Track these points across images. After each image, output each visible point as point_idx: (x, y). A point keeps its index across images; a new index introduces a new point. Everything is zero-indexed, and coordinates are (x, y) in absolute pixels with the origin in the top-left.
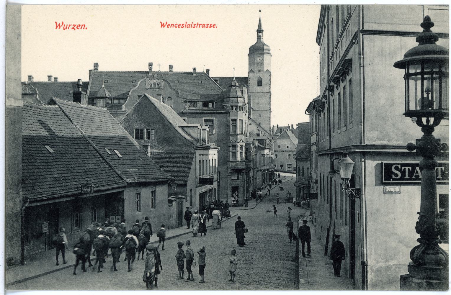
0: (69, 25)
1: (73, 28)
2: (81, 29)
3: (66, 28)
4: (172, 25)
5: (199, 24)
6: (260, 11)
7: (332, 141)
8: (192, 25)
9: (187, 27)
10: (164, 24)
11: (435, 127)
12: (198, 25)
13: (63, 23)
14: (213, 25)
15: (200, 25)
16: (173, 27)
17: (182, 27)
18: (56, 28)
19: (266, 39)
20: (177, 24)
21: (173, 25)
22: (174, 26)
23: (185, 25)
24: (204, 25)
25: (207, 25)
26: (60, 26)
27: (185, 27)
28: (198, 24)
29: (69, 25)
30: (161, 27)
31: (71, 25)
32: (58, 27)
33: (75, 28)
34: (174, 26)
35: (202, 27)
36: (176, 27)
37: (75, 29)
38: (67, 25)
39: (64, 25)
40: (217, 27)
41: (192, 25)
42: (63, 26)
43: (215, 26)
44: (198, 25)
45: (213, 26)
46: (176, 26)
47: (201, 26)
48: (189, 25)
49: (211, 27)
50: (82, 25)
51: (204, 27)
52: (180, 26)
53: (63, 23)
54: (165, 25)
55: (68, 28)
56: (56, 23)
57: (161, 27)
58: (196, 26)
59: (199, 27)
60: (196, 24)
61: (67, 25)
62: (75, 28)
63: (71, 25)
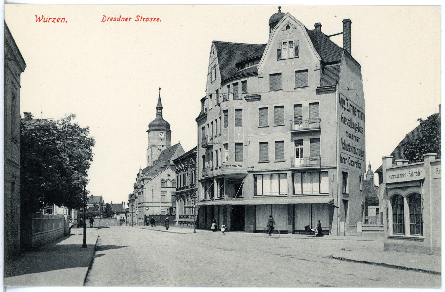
1: (53, 21)
2: (61, 22)
3: (46, 21)
5: (143, 17)
9: (118, 21)
12: (142, 19)
15: (144, 19)
16: (124, 20)
17: (114, 21)
18: (36, 22)
19: (252, 167)
21: (124, 18)
24: (148, 19)
26: (40, 20)
29: (50, 19)
31: (51, 18)
33: (55, 21)
35: (146, 21)
37: (55, 22)
38: (47, 18)
39: (44, 18)
40: (160, 21)
42: (43, 19)
43: (159, 20)
44: (142, 19)
45: (157, 20)
47: (145, 20)
50: (62, 19)
51: (148, 21)
52: (113, 20)
55: (49, 22)
56: (36, 16)
59: (143, 21)
61: (47, 18)
62: (55, 21)
63: (51, 18)
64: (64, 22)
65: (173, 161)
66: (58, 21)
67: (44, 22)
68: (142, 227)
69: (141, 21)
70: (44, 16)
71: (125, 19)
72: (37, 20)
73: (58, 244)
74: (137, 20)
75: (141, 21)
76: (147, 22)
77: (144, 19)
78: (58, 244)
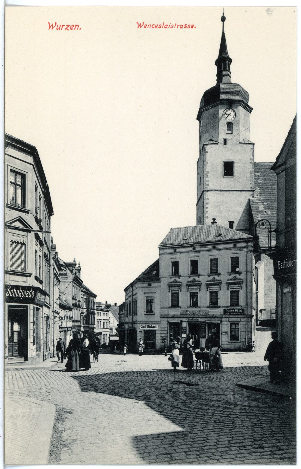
0: (63, 26)
1: (66, 29)
2: (75, 29)
3: (59, 29)
4: (76, 26)
6: (223, 19)
7: (17, 192)
8: (170, 25)
10: (140, 24)
11: (171, 361)
12: (177, 26)
13: (56, 23)
14: (191, 25)
18: (49, 29)
20: (154, 25)
22: (151, 27)
23: (162, 25)
25: (161, 27)
26: (53, 26)
27: (163, 28)
28: (176, 25)
30: (138, 27)
31: (64, 25)
32: (51, 27)
34: (151, 27)
35: (180, 28)
36: (153, 28)
37: (68, 30)
39: (58, 26)
41: (170, 25)
43: (194, 27)
44: (177, 26)
46: (153, 26)
48: (166, 25)
49: (186, 25)
52: (157, 27)
53: (56, 23)
54: (53, 26)
56: (49, 23)
57: (138, 27)
58: (174, 26)
60: (174, 25)
61: (60, 26)
63: (64, 25)
64: (78, 29)
65: (229, 222)
66: (72, 28)
67: (57, 29)
68: (54, 352)
69: (175, 28)
70: (50, 22)
71: (151, 26)
72: (50, 27)
73: (76, 350)
74: (185, 27)
75: (175, 28)
76: (181, 29)
77: (178, 26)
78: (76, 350)
